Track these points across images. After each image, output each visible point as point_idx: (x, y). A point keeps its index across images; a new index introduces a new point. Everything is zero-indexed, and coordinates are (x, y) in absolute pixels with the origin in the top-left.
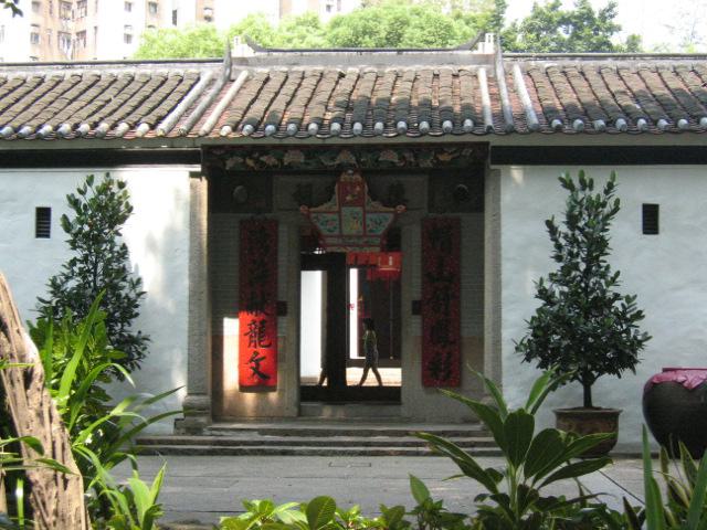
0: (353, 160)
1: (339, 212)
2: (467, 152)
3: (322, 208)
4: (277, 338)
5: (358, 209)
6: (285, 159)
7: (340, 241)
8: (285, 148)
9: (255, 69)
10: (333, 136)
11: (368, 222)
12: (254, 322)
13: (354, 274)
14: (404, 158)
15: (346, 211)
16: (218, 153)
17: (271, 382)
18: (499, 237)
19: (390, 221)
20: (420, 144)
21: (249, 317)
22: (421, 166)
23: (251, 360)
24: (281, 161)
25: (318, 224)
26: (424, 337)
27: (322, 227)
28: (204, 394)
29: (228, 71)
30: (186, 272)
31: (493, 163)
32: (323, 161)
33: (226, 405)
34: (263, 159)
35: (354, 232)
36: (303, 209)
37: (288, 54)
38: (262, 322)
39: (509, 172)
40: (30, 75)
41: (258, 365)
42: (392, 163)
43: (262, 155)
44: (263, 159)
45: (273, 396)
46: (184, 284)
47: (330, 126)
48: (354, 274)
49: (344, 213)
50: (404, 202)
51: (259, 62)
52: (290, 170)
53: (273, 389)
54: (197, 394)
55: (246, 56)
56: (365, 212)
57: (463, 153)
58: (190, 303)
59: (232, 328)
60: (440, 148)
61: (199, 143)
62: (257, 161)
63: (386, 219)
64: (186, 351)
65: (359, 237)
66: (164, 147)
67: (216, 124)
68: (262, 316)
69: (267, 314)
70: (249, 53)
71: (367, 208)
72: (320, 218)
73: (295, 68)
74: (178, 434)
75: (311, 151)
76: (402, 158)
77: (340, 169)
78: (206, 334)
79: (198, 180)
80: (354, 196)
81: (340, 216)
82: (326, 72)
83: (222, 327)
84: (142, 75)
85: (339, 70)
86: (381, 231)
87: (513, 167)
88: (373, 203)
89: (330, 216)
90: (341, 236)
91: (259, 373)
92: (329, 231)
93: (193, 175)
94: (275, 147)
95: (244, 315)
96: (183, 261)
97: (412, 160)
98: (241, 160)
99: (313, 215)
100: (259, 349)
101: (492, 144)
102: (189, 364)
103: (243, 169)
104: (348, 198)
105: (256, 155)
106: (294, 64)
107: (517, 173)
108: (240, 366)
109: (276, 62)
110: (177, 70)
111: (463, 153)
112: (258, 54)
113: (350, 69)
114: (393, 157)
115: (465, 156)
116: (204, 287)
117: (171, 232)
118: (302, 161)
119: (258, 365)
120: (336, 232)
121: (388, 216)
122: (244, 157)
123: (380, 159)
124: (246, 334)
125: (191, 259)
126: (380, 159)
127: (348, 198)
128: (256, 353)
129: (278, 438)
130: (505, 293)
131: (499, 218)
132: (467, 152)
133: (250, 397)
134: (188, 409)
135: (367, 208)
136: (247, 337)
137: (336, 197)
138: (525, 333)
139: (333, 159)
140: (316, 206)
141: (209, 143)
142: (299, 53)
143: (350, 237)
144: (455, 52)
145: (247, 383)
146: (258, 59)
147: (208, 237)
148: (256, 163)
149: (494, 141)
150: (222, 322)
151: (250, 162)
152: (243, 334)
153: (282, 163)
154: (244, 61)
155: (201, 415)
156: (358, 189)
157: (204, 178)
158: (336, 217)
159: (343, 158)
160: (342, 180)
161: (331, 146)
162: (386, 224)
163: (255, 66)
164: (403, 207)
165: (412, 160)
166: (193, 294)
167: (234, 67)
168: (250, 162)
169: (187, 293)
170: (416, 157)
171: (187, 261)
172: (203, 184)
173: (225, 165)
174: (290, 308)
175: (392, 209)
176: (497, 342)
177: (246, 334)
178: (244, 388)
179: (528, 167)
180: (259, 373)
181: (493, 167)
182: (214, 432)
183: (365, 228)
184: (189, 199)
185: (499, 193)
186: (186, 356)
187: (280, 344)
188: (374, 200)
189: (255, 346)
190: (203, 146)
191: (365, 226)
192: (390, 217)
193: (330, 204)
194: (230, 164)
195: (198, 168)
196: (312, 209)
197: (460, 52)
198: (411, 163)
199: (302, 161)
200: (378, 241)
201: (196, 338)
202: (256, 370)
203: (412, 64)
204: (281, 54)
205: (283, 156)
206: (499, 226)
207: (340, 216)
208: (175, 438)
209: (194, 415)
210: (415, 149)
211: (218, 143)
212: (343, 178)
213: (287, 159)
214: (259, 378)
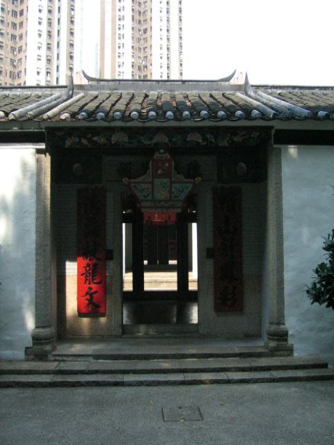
0: (166, 140)
1: (152, 183)
2: (255, 134)
3: (140, 179)
4: (106, 276)
5: (166, 180)
6: (112, 139)
7: (153, 204)
8: (113, 130)
9: (89, 92)
10: (151, 120)
11: (173, 190)
12: (88, 265)
13: (194, 226)
14: (206, 139)
15: (157, 181)
16: (59, 134)
17: (101, 310)
18: (281, 200)
19: (190, 189)
20: (219, 128)
21: (85, 261)
22: (220, 145)
23: (87, 294)
24: (109, 140)
25: (136, 192)
26: (215, 274)
27: (138, 194)
28: (50, 326)
29: (71, 92)
30: (34, 229)
31: (275, 143)
32: (143, 141)
33: (68, 326)
34: (95, 139)
35: (163, 198)
36: (125, 180)
37: (111, 82)
38: (95, 265)
39: (286, 150)
40: (160, 360)
41: (92, 297)
42: (197, 142)
43: (93, 136)
44: (95, 139)
45: (103, 320)
46: (32, 237)
47: (147, 115)
48: (194, 226)
49: (156, 183)
50: (200, 175)
51: (91, 87)
52: (116, 150)
53: (103, 315)
54: (43, 327)
55: (83, 83)
56: (172, 183)
57: (252, 136)
58: (37, 254)
59: (72, 269)
60: (234, 131)
61: (43, 125)
62: (90, 141)
63: (187, 188)
64: (34, 293)
65: (166, 201)
66: (15, 129)
67: (60, 112)
68: (95, 261)
69: (98, 259)
70: (85, 82)
71: (173, 179)
72: (138, 187)
73: (115, 91)
74: (27, 360)
75: (132, 132)
76: (205, 139)
77: (156, 148)
78: (50, 278)
79: (43, 155)
80: (164, 170)
81: (153, 186)
82: (136, 94)
83: (65, 269)
84: (13, 95)
85: (144, 92)
86: (183, 196)
87: (292, 146)
88: (178, 176)
89: (144, 186)
90: (153, 200)
91: (93, 304)
92: (145, 197)
93: (39, 151)
94: (105, 128)
95: (80, 259)
96: (31, 222)
97: (213, 141)
98: (77, 140)
99: (133, 185)
100: (93, 286)
101: (276, 128)
102: (36, 303)
103: (78, 147)
104: (159, 172)
105: (89, 136)
106: (115, 89)
107: (293, 150)
108: (78, 299)
109: (103, 87)
110: (37, 93)
111: (252, 136)
112: (90, 83)
113: (151, 92)
114: (198, 138)
115: (253, 138)
116: (48, 241)
117: (19, 197)
118: (126, 140)
119: (92, 297)
120: (149, 198)
121: (188, 185)
122: (80, 137)
123: (188, 139)
124: (82, 275)
125: (37, 218)
126: (188, 139)
127: (159, 172)
128: (90, 288)
129: (119, 378)
130: (286, 244)
131: (281, 186)
132: (255, 134)
133: (85, 320)
134: (37, 339)
135: (173, 179)
136: (83, 276)
137: (150, 171)
138: (310, 278)
139: (151, 139)
140: (135, 178)
141: (52, 125)
142: (118, 82)
143: (160, 201)
144: (219, 83)
145: (84, 310)
146: (91, 86)
147: (51, 207)
148: (89, 142)
149: (278, 125)
150: (64, 265)
151: (84, 141)
152: (80, 274)
153: (111, 142)
154: (81, 87)
155: (47, 344)
156: (167, 165)
157: (47, 154)
158: (150, 186)
159: (160, 138)
160: (155, 157)
161: (148, 128)
162: (187, 191)
163: (89, 90)
164: (200, 178)
165: (213, 141)
166: (40, 247)
167: (75, 91)
168: (84, 141)
169: (34, 246)
170: (216, 138)
171: (34, 220)
172: (47, 160)
173: (65, 143)
174: (115, 254)
175: (192, 180)
176: (280, 282)
177: (82, 275)
178: (81, 314)
179: (303, 146)
180: (93, 304)
181: (275, 146)
182: (57, 358)
183: (171, 196)
184: (35, 171)
185: (281, 167)
186: (34, 296)
187: (108, 280)
188: (178, 173)
189: (89, 284)
190: (46, 128)
191: (170, 192)
192: (190, 186)
193: (144, 176)
194: (68, 143)
195: (43, 146)
196: (132, 180)
197: (223, 83)
198: (211, 142)
199: (126, 140)
200: (180, 204)
201: (42, 282)
202: (91, 302)
203: (192, 90)
204: (106, 83)
205: (111, 136)
206: (281, 192)
207: (153, 186)
208: (26, 366)
209: (42, 344)
210: (215, 131)
211: (58, 125)
212: (156, 156)
213: (114, 139)
214: (91, 306)
